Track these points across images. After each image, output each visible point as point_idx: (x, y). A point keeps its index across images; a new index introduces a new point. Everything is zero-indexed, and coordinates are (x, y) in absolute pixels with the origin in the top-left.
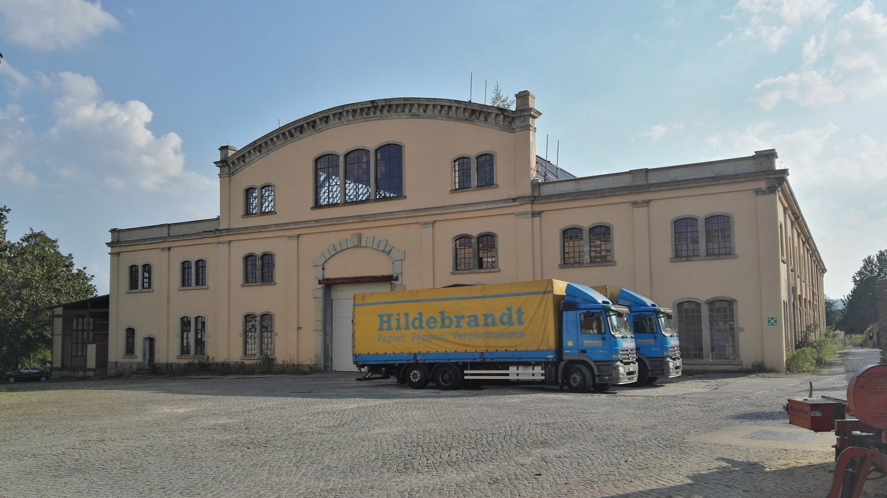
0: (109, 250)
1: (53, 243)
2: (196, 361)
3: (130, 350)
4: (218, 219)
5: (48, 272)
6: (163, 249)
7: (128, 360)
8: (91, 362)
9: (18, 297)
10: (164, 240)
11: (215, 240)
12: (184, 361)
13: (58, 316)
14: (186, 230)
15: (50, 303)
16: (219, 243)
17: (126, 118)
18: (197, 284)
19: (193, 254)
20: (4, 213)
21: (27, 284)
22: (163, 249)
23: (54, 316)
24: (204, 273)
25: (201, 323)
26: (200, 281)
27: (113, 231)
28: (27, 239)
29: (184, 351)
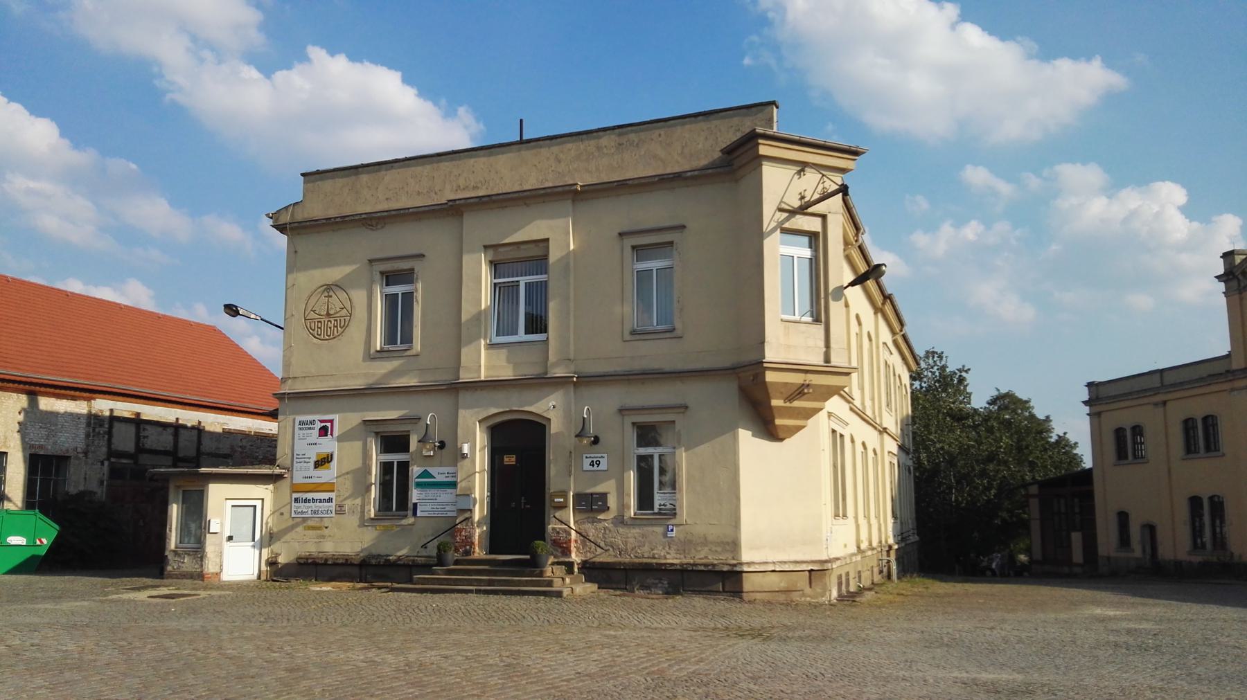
0: (1087, 409)
1: (1024, 404)
2: (1215, 559)
3: (1124, 540)
4: (1228, 356)
5: (1019, 441)
6: (1156, 404)
7: (1122, 555)
8: (1078, 556)
9: (984, 473)
10: (1156, 391)
11: (1226, 386)
12: (1197, 559)
13: (1033, 496)
14: (1113, 391)
15: (1023, 479)
16: (1233, 390)
17: (1156, 208)
18: (1208, 449)
19: (1197, 407)
20: (964, 374)
21: (991, 458)
22: (1156, 404)
23: (1028, 496)
24: (1216, 434)
25: (1217, 506)
26: (1212, 445)
27: (1090, 385)
28: (993, 402)
29: (1197, 546)
